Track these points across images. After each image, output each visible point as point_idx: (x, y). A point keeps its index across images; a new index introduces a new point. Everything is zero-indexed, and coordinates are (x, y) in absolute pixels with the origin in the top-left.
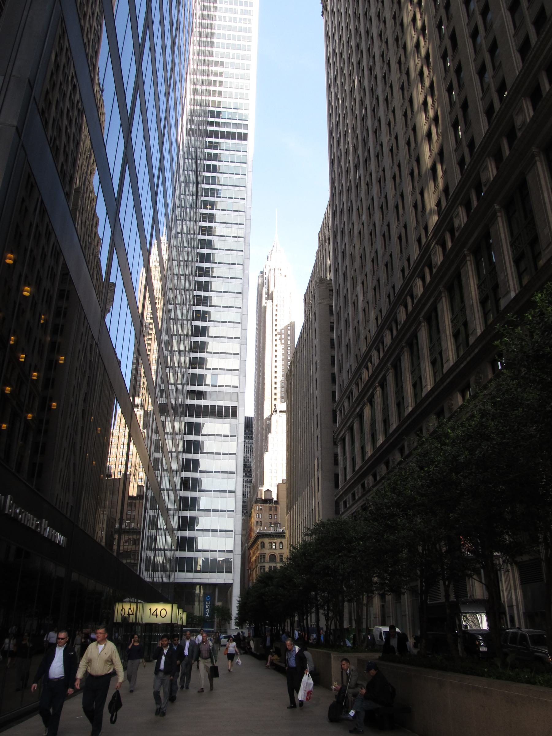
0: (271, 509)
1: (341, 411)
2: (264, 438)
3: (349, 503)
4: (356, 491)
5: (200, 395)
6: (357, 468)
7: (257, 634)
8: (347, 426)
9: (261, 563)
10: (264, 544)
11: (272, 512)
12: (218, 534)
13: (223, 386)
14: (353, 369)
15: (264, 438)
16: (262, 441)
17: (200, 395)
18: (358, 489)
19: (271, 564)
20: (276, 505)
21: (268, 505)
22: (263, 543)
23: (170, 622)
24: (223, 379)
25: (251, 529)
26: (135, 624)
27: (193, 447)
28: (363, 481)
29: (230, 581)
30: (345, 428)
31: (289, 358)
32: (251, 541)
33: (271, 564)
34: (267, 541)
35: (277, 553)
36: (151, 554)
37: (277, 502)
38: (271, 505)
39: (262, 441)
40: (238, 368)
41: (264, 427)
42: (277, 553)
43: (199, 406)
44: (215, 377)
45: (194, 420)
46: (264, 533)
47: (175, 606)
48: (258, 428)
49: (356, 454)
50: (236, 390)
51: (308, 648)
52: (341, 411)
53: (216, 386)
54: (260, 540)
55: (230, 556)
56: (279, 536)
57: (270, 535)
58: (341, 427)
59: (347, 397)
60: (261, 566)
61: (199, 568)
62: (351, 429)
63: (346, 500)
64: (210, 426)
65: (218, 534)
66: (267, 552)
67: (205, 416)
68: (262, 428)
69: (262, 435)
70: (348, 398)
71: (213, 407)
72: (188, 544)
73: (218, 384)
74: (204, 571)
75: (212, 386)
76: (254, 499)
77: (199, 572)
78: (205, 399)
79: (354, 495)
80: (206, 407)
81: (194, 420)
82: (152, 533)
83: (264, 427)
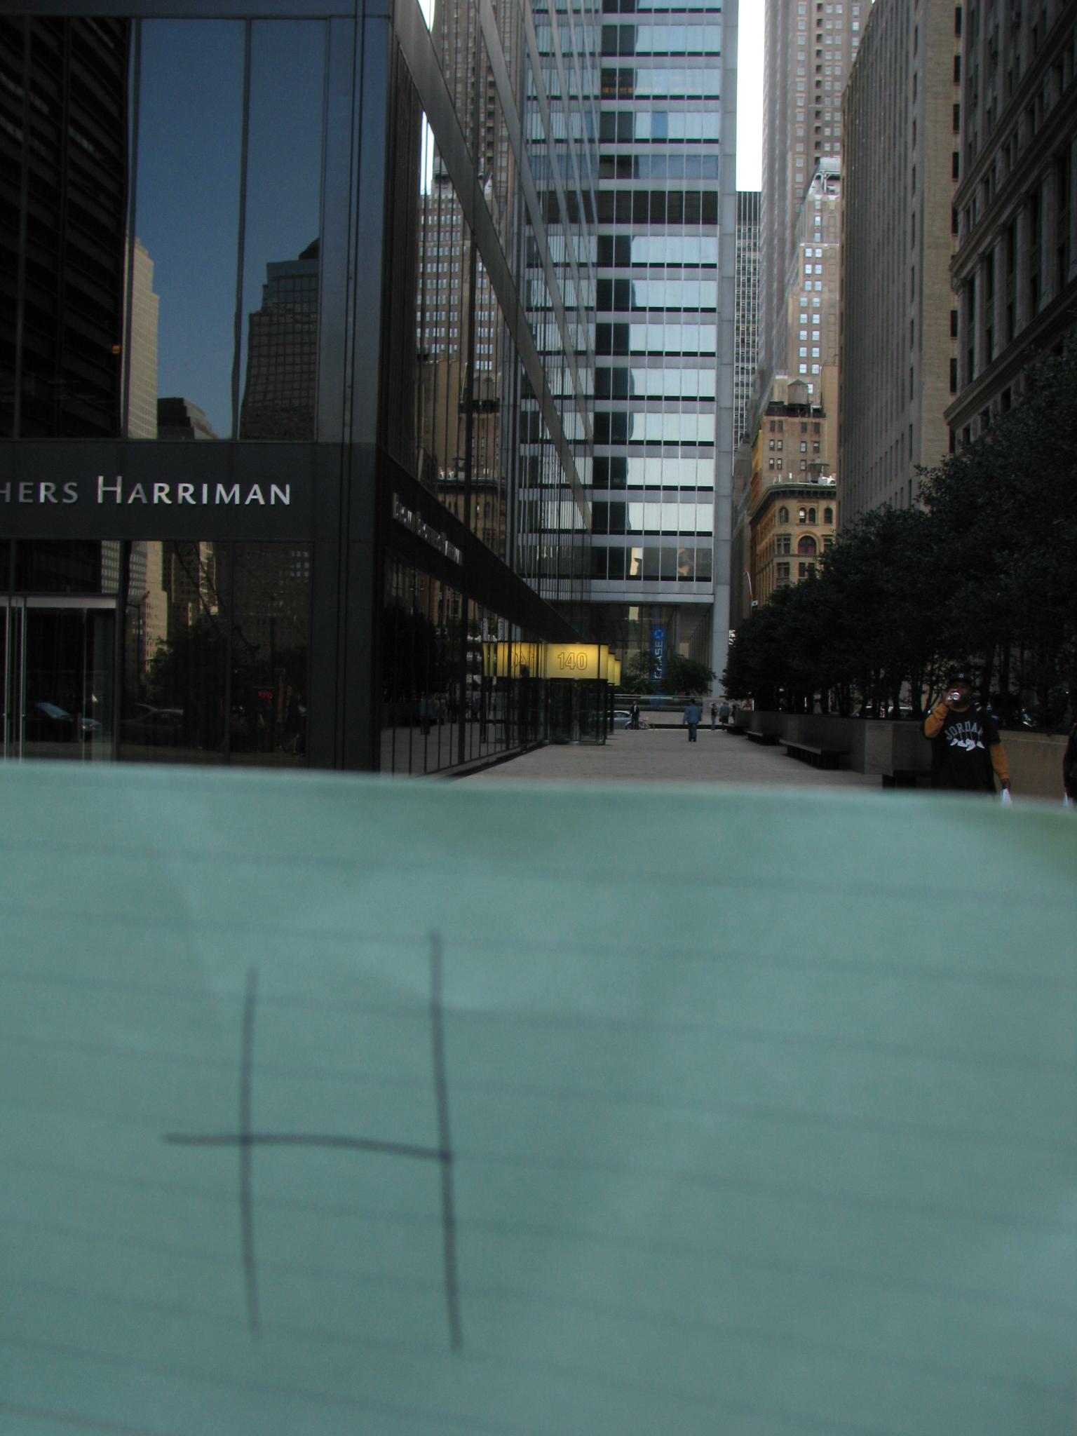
0: (804, 427)
1: (987, 182)
2: (788, 249)
3: (975, 434)
4: (1013, 389)
5: (625, 166)
6: (1043, 305)
7: (764, 704)
8: (981, 250)
9: (779, 555)
10: (787, 512)
11: (807, 437)
12: (675, 496)
13: (680, 141)
14: (1050, 23)
15: (788, 249)
16: (782, 254)
17: (625, 166)
18: (1017, 384)
19: (802, 560)
20: (817, 420)
21: (797, 420)
22: (784, 510)
23: (595, 677)
24: (683, 124)
25: (756, 477)
26: (537, 680)
27: (615, 296)
28: (1006, 387)
29: (708, 599)
30: (975, 257)
31: (856, 26)
32: (754, 507)
33: (802, 560)
34: (792, 505)
35: (819, 534)
36: (533, 539)
37: (819, 413)
38: (805, 420)
39: (782, 254)
40: (712, 349)
41: (788, 219)
42: (819, 534)
43: (623, 195)
44: (660, 116)
45: (614, 230)
46: (787, 486)
47: (604, 650)
48: (771, 223)
49: (1044, 266)
50: (714, 149)
51: (418, 513)
52: (968, 212)
53: (663, 141)
54: (778, 504)
55: (708, 543)
56: (822, 493)
57: (801, 493)
58: (1013, 184)
59: (1025, 108)
60: (779, 564)
61: (633, 571)
62: (988, 259)
63: (1009, 390)
64: (648, 245)
65: (675, 496)
66: (797, 532)
67: (640, 219)
68: (782, 223)
69: (782, 241)
70: (986, 182)
71: (658, 195)
72: (610, 518)
73: (671, 136)
74: (648, 575)
75: (655, 141)
76: (764, 405)
77: (637, 578)
78: (637, 176)
79: (1006, 396)
80: (641, 195)
81: (614, 230)
82: (534, 494)
83: (788, 219)
